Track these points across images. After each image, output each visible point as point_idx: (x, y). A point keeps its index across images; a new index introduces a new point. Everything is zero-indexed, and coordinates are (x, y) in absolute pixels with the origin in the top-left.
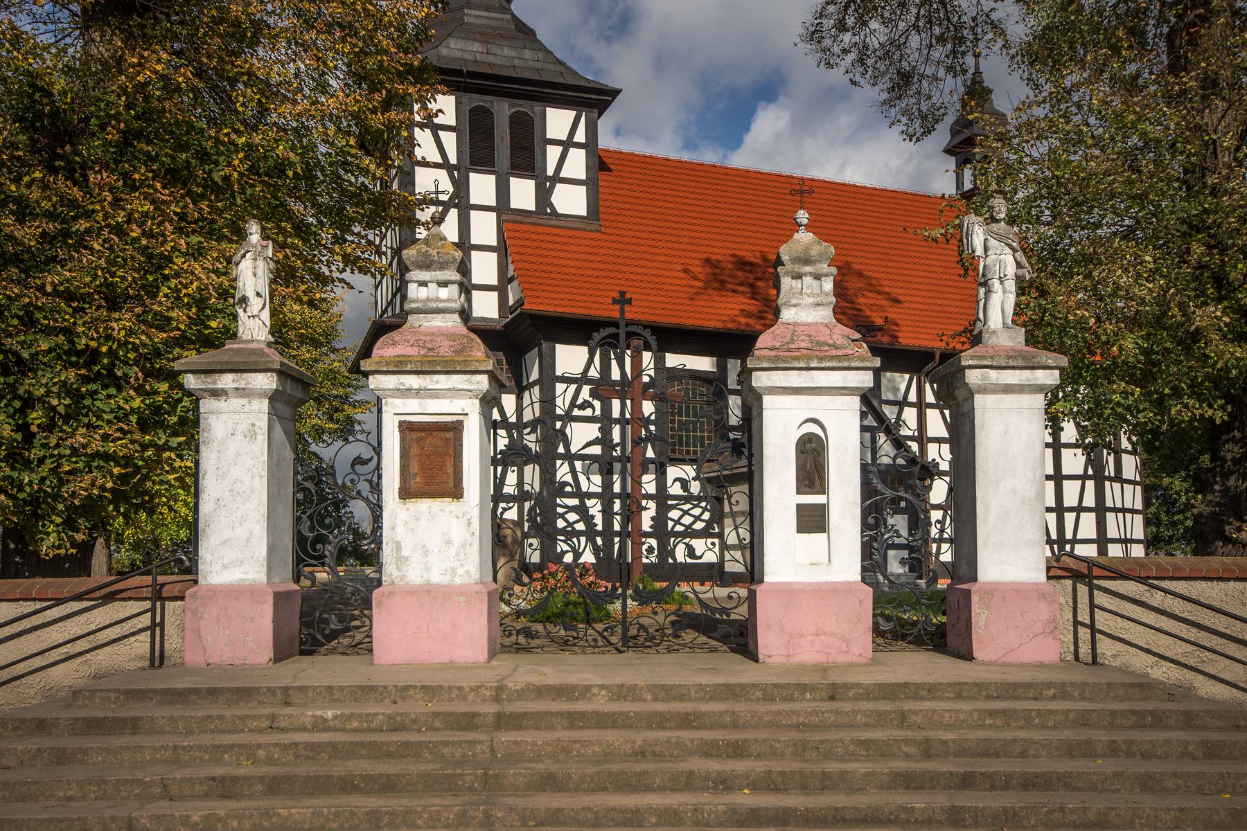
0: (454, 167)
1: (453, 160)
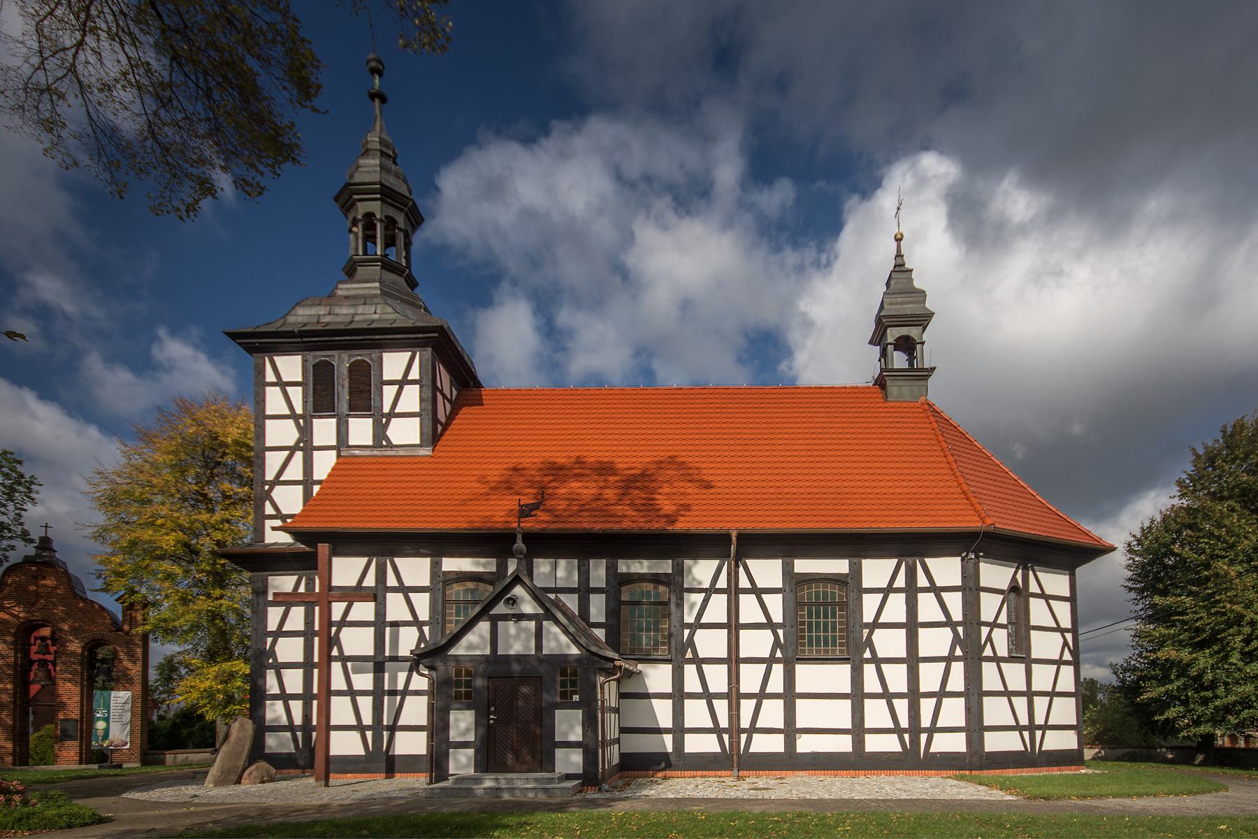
0: (300, 416)
1: (299, 411)
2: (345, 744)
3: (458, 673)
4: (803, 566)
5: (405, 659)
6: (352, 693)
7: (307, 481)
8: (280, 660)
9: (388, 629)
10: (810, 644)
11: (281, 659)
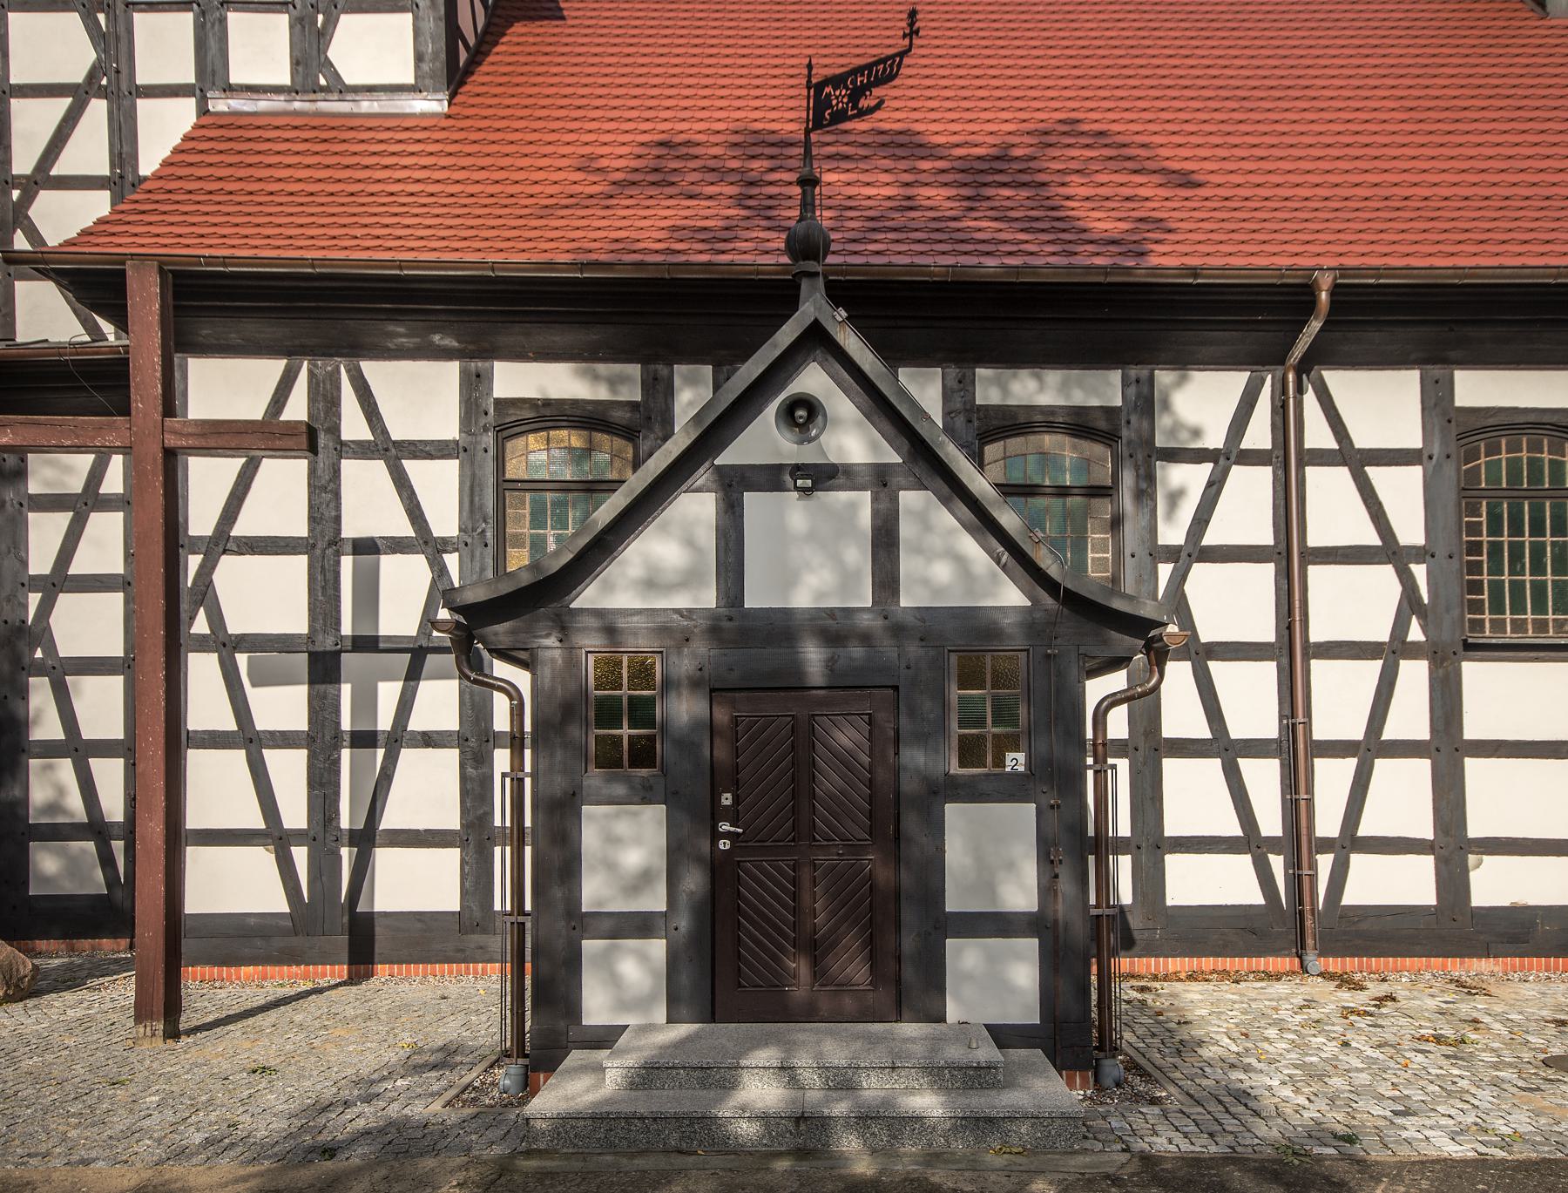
2: (234, 884)
3: (609, 673)
4: (1478, 389)
5: (396, 646)
6: (250, 740)
7: (121, 179)
8: (63, 652)
9: (347, 562)
10: (1497, 607)
11: (67, 648)
